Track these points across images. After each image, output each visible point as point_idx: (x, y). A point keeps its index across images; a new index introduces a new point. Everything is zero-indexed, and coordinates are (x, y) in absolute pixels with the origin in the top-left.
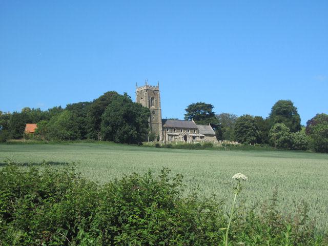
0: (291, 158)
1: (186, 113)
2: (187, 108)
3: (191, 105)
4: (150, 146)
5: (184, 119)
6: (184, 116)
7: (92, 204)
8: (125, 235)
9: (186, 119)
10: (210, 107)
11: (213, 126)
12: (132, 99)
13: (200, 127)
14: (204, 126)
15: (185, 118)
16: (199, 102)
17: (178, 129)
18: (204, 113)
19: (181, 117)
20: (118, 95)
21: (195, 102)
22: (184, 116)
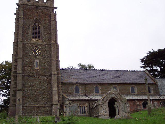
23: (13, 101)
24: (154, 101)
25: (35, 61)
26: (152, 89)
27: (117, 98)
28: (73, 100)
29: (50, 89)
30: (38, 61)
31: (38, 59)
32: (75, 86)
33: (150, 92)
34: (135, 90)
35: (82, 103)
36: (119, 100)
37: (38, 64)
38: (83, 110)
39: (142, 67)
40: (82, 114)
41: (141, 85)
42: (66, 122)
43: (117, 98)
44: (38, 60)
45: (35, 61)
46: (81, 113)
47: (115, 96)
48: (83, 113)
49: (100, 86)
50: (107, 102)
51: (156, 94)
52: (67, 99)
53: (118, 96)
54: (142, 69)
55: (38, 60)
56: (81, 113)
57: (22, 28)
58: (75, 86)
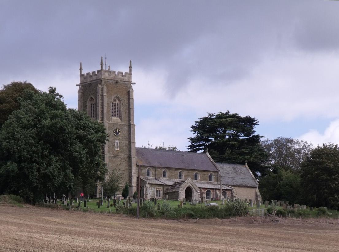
0: (249, 227)
1: (194, 136)
2: (194, 124)
3: (206, 119)
4: (216, 168)
5: (187, 150)
6: (190, 143)
7: (118, 131)
8: (49, 121)
9: (193, 148)
10: (250, 122)
11: (254, 167)
12: (64, 100)
13: (225, 169)
14: (234, 166)
15: (191, 147)
16: (224, 112)
17: (208, 156)
18: (234, 137)
19: (183, 146)
20: (36, 92)
21: (216, 112)
22: (190, 143)
23: (36, 171)
24: (216, 190)
25: (116, 142)
26: (213, 177)
27: (192, 186)
28: (151, 184)
29: (130, 170)
30: (118, 142)
31: (118, 140)
32: (147, 169)
33: (211, 179)
34: (198, 177)
35: (158, 187)
36: (193, 188)
37: (118, 145)
38: (158, 193)
39: (189, 149)
40: (158, 197)
41: (204, 172)
42: (287, 224)
43: (192, 186)
44: (118, 141)
45: (116, 141)
46: (156, 196)
47: (191, 185)
48: (158, 196)
49: (168, 170)
50: (185, 189)
51: (217, 182)
52: (147, 183)
53: (193, 185)
54: (190, 150)
55: (118, 141)
56: (156, 196)
57: (106, 107)
58: (147, 169)
